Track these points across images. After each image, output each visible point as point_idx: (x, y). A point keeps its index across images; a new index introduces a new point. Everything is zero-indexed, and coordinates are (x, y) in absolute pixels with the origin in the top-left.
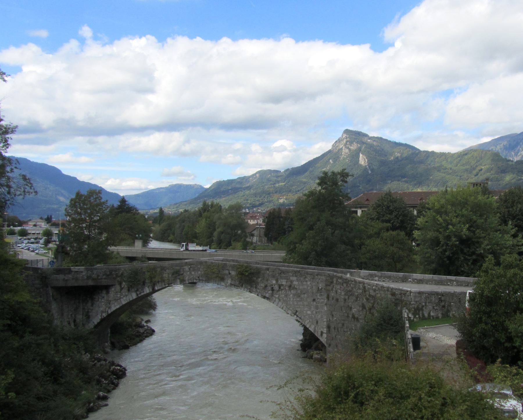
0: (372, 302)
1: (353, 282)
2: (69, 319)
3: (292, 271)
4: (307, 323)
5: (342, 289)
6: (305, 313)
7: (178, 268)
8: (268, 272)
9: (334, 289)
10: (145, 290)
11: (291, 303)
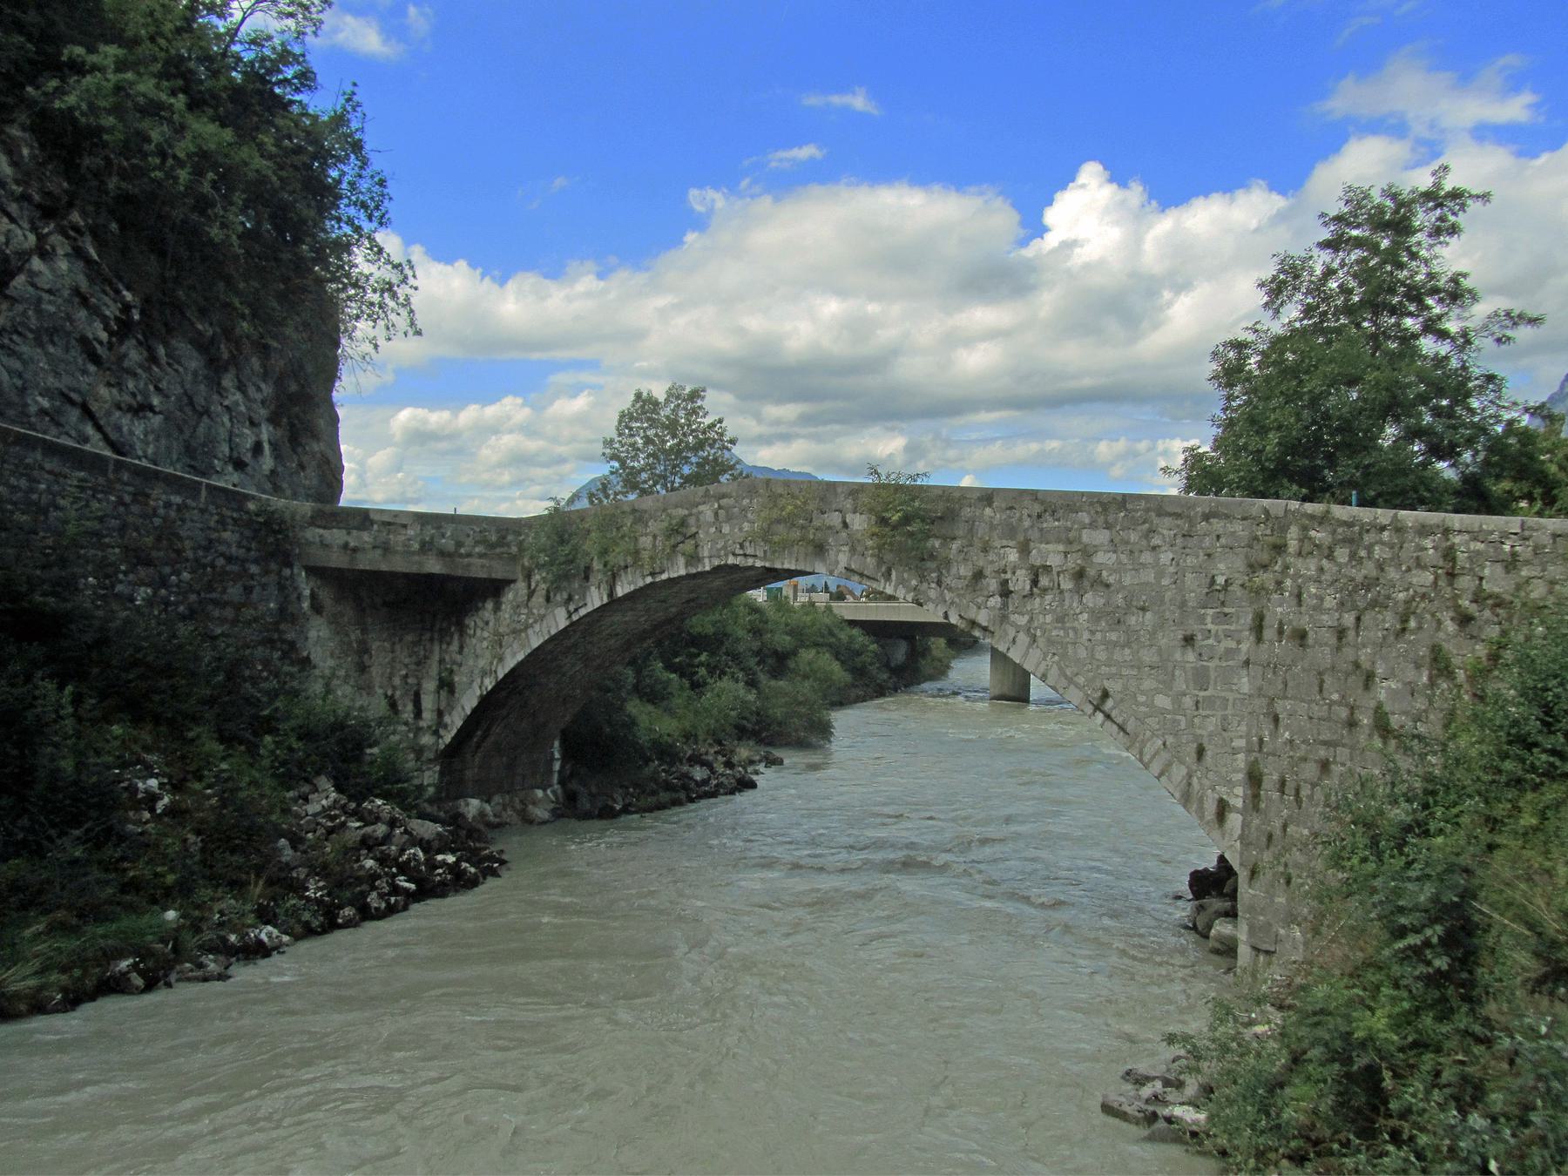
0: (1493, 632)
1: (1386, 534)
2: (394, 688)
3: (1091, 504)
4: (1153, 757)
5: (1326, 577)
6: (1143, 704)
7: (682, 512)
8: (988, 511)
9: (1288, 582)
10: (588, 600)
11: (1083, 653)
